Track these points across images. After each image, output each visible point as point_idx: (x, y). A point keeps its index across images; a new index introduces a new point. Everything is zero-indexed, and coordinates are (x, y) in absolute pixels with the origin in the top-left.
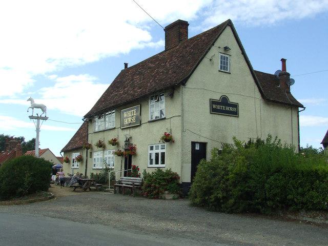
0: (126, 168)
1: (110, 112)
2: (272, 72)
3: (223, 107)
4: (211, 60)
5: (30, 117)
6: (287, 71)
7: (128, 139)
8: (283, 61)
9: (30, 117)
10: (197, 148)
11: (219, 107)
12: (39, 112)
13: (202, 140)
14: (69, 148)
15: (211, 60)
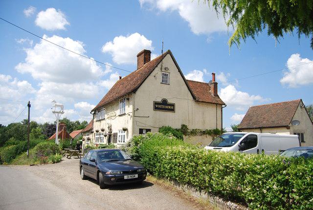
3: (164, 106)
8: (214, 74)
11: (159, 106)
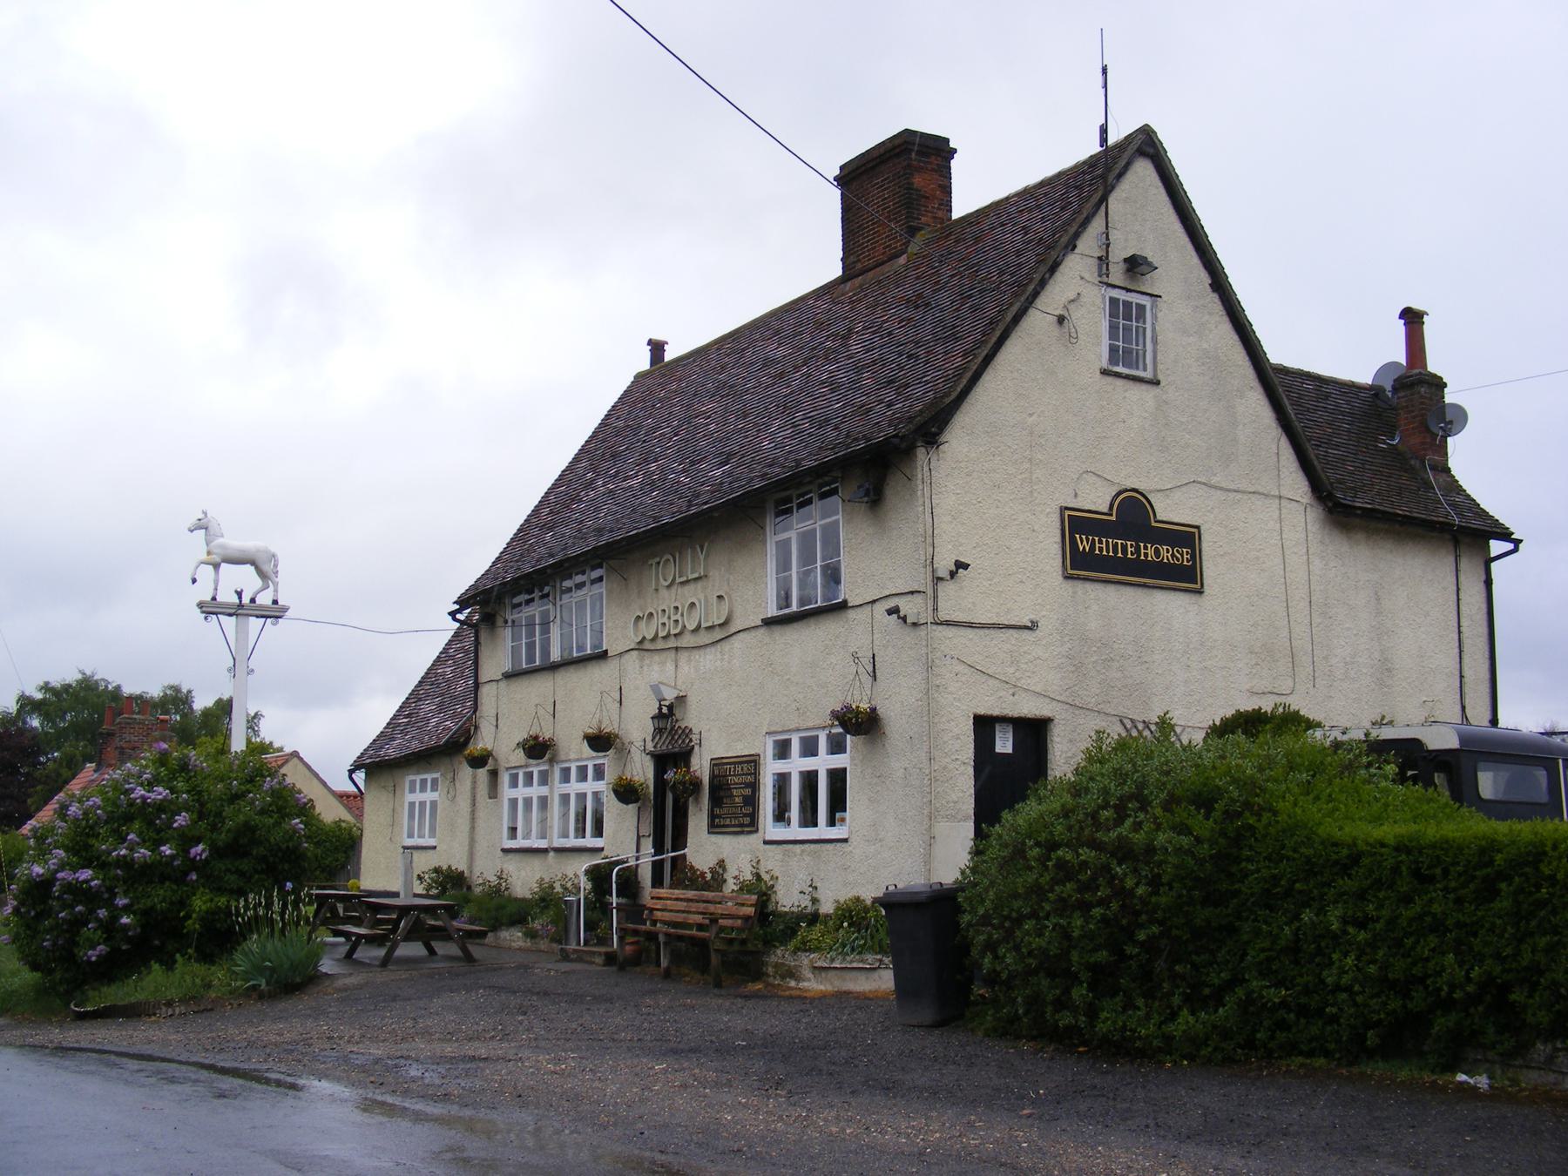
0: (659, 847)
1: (579, 579)
2: (1362, 373)
3: (1128, 545)
4: (1061, 320)
5: (201, 605)
6: (1433, 366)
7: (670, 707)
8: (1412, 318)
9: (201, 605)
10: (1004, 744)
11: (1104, 546)
12: (243, 579)
13: (1028, 708)
14: (391, 751)
15: (1061, 320)
